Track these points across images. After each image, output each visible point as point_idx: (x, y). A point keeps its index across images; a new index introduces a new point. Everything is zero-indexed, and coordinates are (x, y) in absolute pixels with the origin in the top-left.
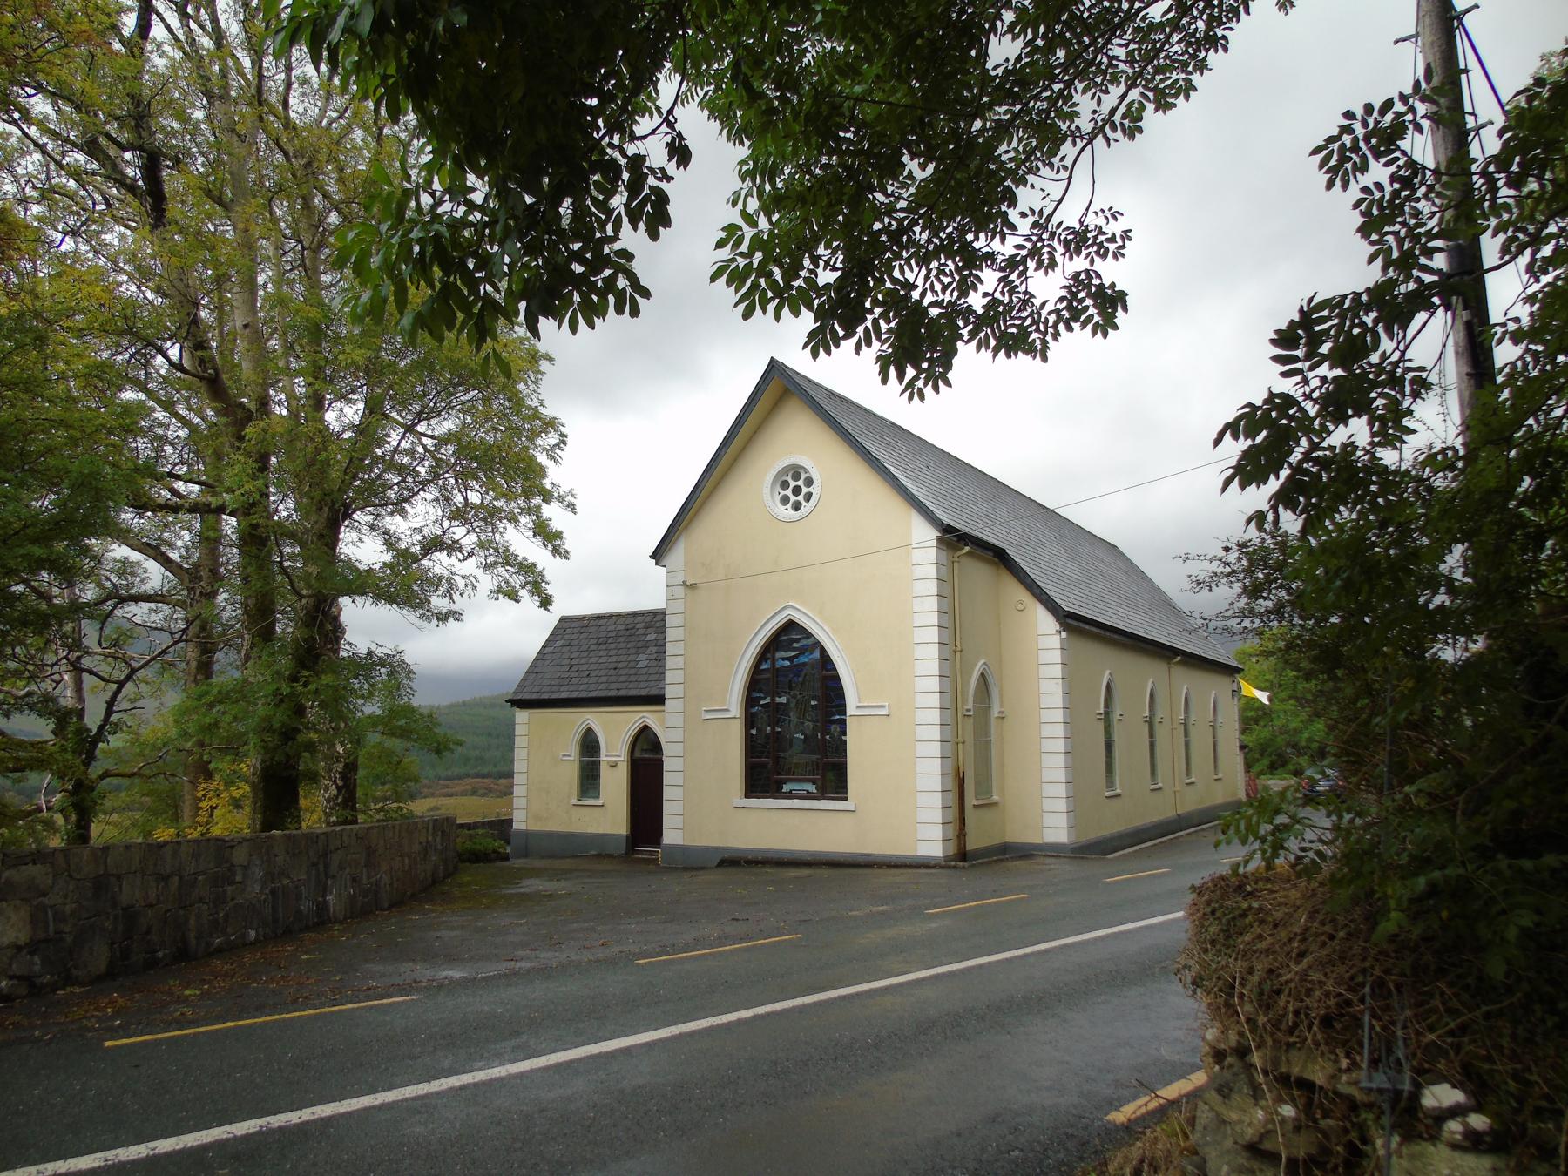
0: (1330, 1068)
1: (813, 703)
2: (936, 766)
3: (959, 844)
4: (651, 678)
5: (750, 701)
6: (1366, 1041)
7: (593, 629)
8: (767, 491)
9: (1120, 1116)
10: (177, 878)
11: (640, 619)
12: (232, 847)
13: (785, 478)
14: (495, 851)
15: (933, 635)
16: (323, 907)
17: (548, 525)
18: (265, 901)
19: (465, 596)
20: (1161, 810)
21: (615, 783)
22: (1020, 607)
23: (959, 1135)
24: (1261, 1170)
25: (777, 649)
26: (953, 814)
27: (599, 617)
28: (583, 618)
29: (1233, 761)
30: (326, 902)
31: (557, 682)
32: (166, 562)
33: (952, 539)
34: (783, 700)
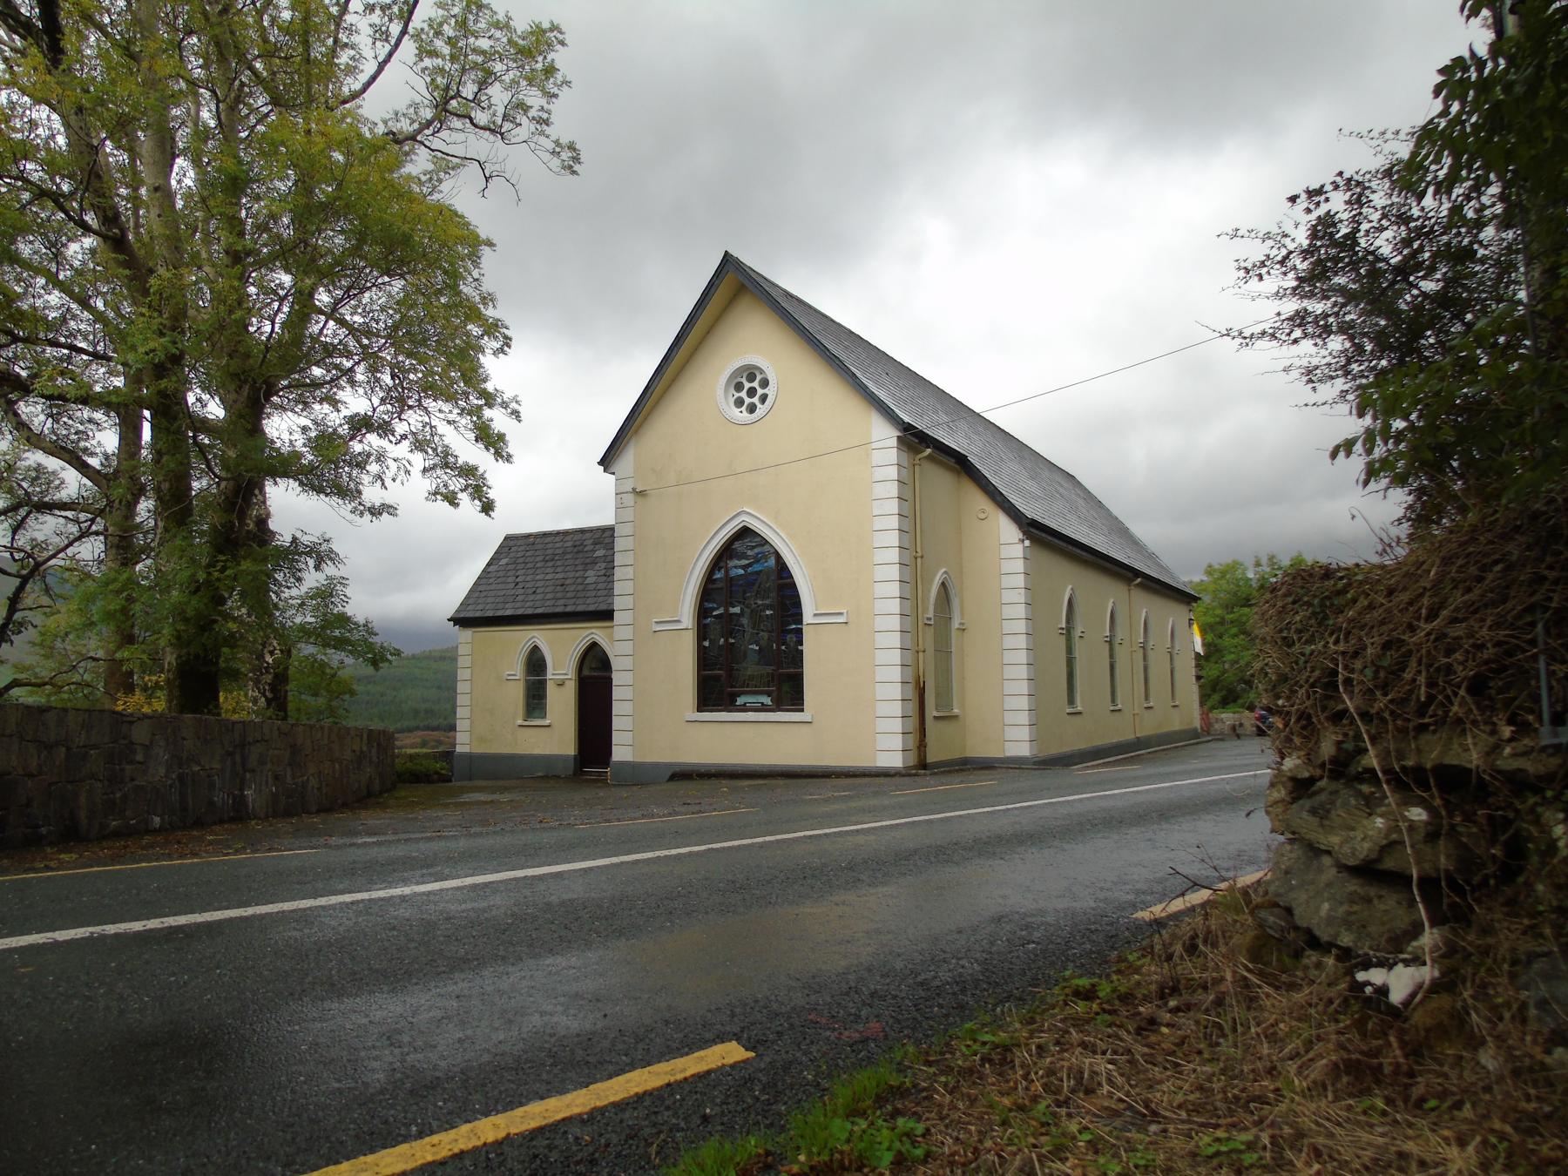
0: (1487, 740)
1: (768, 612)
2: (896, 674)
3: (919, 755)
4: (599, 593)
5: (702, 612)
6: (1544, 693)
7: (540, 547)
8: (720, 391)
9: (1144, 915)
10: (63, 749)
11: (588, 535)
12: (131, 723)
13: (739, 380)
14: (436, 773)
15: (893, 539)
16: (240, 801)
17: (475, 258)
18: (171, 786)
19: (398, 481)
20: (1122, 732)
21: (562, 702)
22: (982, 516)
23: (960, 932)
24: (1380, 897)
25: (731, 558)
26: (913, 724)
27: (545, 535)
28: (528, 536)
29: (1189, 691)
30: (243, 796)
31: (502, 599)
32: (83, 468)
33: (914, 440)
34: (737, 610)
